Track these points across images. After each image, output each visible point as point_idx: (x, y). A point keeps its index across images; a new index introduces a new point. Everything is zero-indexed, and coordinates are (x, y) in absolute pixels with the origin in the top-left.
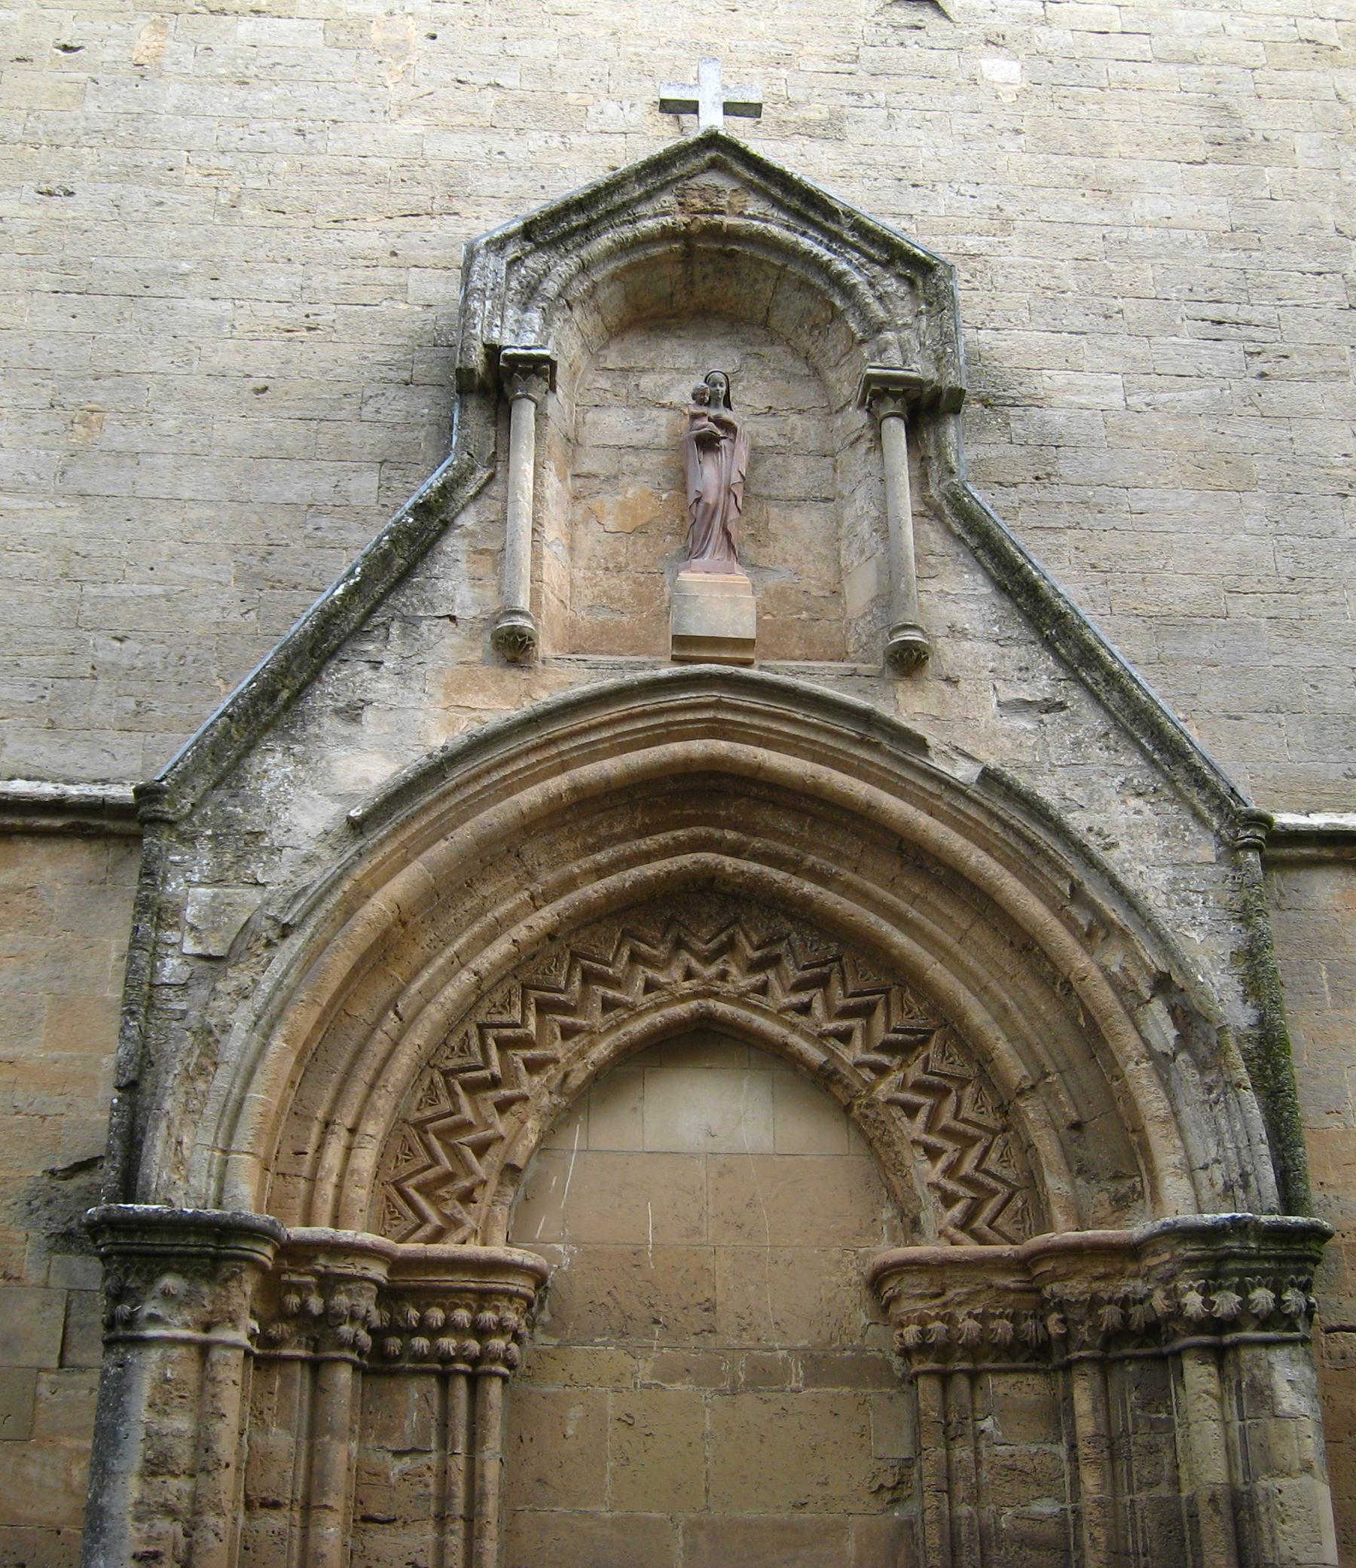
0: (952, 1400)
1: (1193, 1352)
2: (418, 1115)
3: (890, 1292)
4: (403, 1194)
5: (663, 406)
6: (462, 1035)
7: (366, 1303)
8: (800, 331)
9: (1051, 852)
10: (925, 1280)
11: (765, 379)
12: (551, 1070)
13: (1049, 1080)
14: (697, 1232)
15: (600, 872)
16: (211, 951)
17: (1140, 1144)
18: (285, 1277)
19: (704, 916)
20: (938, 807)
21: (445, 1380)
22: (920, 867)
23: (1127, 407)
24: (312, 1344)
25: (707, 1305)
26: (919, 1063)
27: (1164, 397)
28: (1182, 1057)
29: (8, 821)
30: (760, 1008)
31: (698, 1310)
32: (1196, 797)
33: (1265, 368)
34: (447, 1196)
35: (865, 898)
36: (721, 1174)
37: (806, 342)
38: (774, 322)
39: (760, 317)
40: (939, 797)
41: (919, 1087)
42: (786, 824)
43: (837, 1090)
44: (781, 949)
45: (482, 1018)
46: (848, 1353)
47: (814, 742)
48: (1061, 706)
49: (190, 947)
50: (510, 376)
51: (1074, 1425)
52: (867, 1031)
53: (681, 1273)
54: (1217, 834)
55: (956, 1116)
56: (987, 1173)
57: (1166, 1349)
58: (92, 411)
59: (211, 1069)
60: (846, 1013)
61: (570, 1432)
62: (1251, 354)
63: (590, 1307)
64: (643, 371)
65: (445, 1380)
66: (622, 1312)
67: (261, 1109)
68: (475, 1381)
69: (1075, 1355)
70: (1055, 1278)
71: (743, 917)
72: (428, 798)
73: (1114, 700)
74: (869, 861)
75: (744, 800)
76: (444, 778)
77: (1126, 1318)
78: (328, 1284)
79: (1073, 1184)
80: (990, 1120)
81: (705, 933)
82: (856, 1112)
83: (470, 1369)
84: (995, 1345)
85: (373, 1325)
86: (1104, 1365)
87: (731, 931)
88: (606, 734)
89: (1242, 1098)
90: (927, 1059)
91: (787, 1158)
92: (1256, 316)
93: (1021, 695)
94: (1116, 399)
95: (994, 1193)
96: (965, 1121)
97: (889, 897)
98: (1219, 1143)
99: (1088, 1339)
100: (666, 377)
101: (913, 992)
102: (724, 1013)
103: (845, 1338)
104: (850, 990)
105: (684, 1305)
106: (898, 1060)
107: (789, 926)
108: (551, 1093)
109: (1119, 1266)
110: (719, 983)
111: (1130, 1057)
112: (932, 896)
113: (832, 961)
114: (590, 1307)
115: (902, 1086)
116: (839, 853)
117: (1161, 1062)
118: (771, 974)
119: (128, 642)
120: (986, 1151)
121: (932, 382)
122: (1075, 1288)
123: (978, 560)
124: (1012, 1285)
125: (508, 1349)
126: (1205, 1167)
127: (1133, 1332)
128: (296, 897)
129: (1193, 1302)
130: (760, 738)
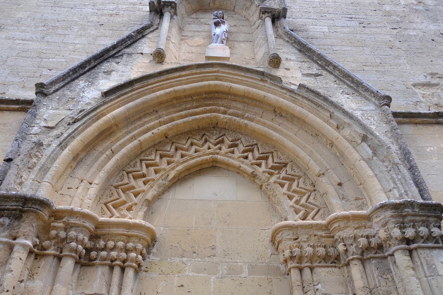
0: (304, 278)
1: (400, 251)
2: (117, 184)
3: (279, 239)
4: (107, 208)
5: (207, 24)
6: (134, 162)
7: (84, 237)
8: (243, 10)
9: (323, 105)
10: (291, 232)
11: (234, 20)
12: (163, 172)
13: (329, 171)
14: (210, 223)
15: (182, 117)
16: (49, 125)
17: (364, 188)
18: (52, 224)
19: (214, 133)
20: (286, 97)
21: (112, 268)
22: (281, 116)
23: (329, 32)
24: (59, 249)
25: (213, 247)
26: (284, 172)
27: (339, 30)
28: (375, 158)
29: (2, 106)
30: (232, 157)
31: (210, 249)
32: (366, 94)
33: (365, 26)
34: (123, 208)
35: (264, 124)
36: (219, 206)
37: (244, 13)
38: (236, 10)
39: (232, 9)
40: (286, 94)
41: (284, 179)
42: (239, 106)
43: (257, 181)
44: (238, 142)
45: (142, 157)
46: (264, 264)
47: (247, 81)
48: (320, 75)
49: (43, 124)
50: (164, 7)
51: (353, 286)
52: (267, 164)
53: (204, 237)
54: (374, 103)
55: (298, 186)
56: (310, 203)
57: (386, 254)
58: (55, 27)
59: (40, 156)
60: (259, 159)
61: (160, 291)
62: (361, 23)
63: (171, 247)
64: (201, 18)
65: (112, 268)
66: (182, 249)
67: (55, 169)
68: (123, 269)
69: (351, 257)
70: (340, 229)
71: (227, 134)
72: (127, 90)
73: (337, 73)
74: (265, 114)
75: (227, 100)
76: (133, 85)
77: (369, 243)
78: (68, 227)
79: (341, 202)
80: (310, 188)
81: (215, 137)
82: (264, 187)
83: (122, 264)
84: (319, 257)
85: (87, 246)
86: (363, 261)
87: (223, 137)
88: (184, 78)
89: (399, 168)
90: (287, 171)
91: (241, 202)
92: (360, 17)
93: (309, 72)
94: (327, 30)
95: (313, 209)
96: (300, 188)
97: (272, 124)
98: (394, 182)
99: (355, 251)
100: (207, 20)
101: (281, 153)
102: (220, 158)
103: (263, 259)
104: (260, 152)
105: (204, 247)
106: (277, 172)
107: (241, 136)
108: (162, 180)
109: (363, 224)
110: (219, 150)
111: (357, 160)
112: (285, 123)
113: (254, 145)
114: (171, 247)
115: (279, 178)
116: (256, 113)
117: (368, 161)
118: (236, 148)
119: (52, 71)
120: (309, 197)
121: (278, 8)
122: (348, 232)
123: (294, 46)
124: (324, 235)
125: (137, 257)
126: (390, 190)
127: (373, 247)
128: (81, 111)
129: (397, 232)
130: (231, 81)
